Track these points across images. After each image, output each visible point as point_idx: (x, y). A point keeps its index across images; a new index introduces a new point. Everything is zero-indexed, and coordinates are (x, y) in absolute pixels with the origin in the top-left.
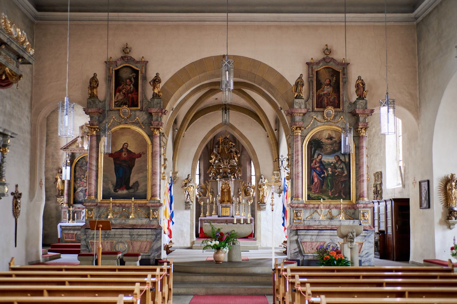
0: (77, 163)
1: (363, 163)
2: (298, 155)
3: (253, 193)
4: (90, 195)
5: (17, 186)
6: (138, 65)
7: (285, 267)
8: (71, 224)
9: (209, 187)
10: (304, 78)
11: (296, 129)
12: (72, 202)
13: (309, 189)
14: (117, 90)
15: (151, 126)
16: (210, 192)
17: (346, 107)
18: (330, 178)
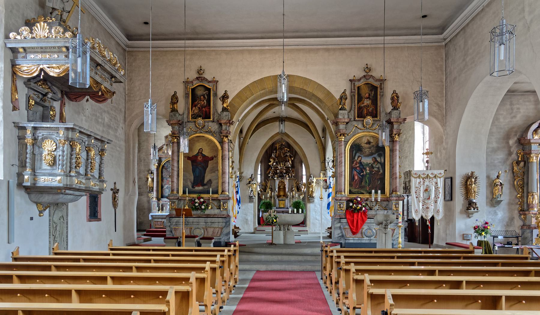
0: (163, 166)
1: (396, 163)
2: (341, 157)
3: (303, 189)
4: (172, 191)
5: (115, 183)
6: (211, 84)
7: (331, 248)
8: (160, 213)
9: (269, 185)
10: (348, 93)
11: (340, 135)
12: (160, 197)
13: (351, 185)
14: (193, 105)
15: (222, 136)
16: (270, 188)
17: (383, 118)
18: (368, 176)
